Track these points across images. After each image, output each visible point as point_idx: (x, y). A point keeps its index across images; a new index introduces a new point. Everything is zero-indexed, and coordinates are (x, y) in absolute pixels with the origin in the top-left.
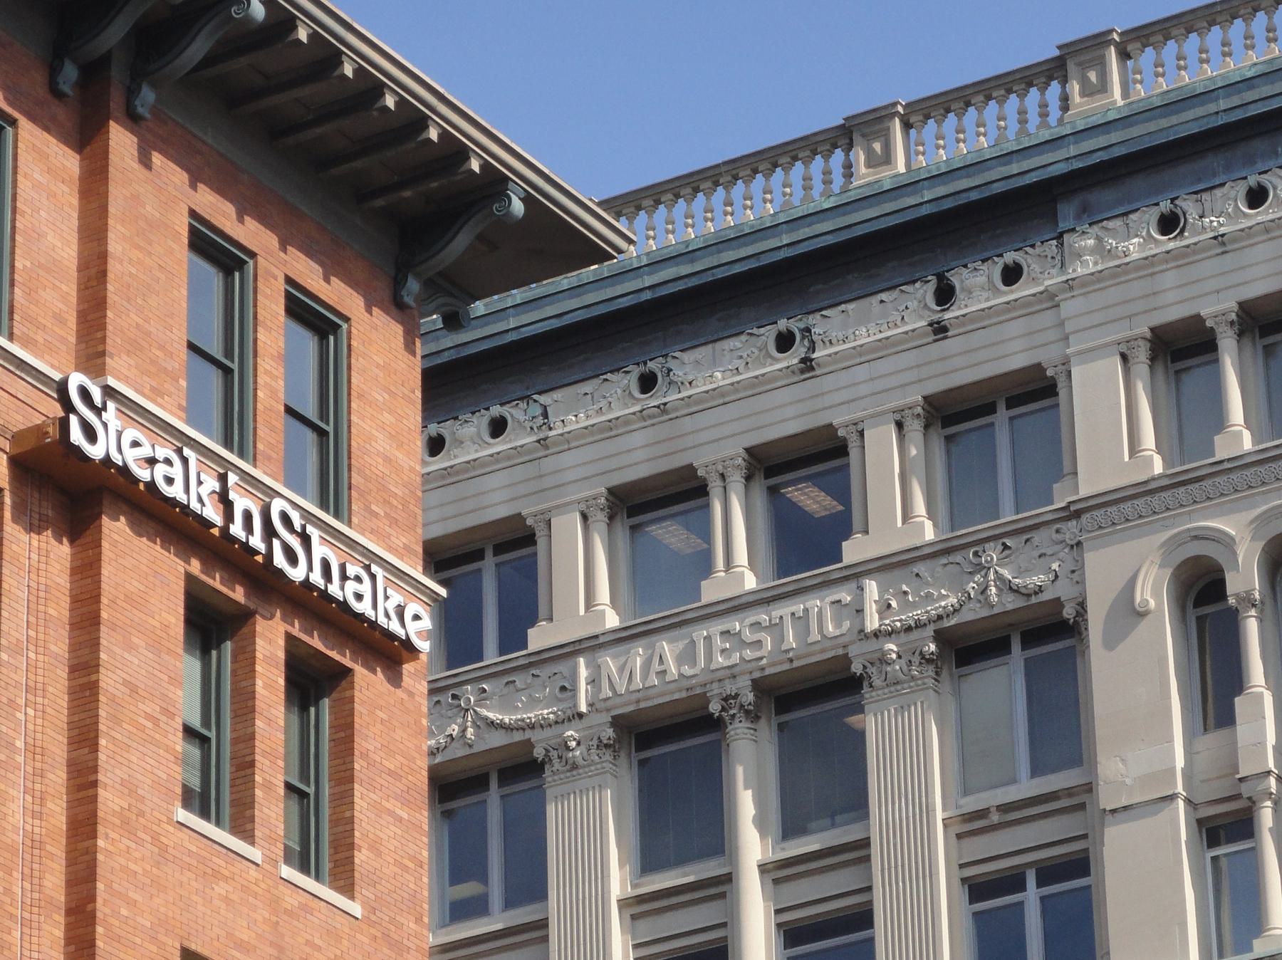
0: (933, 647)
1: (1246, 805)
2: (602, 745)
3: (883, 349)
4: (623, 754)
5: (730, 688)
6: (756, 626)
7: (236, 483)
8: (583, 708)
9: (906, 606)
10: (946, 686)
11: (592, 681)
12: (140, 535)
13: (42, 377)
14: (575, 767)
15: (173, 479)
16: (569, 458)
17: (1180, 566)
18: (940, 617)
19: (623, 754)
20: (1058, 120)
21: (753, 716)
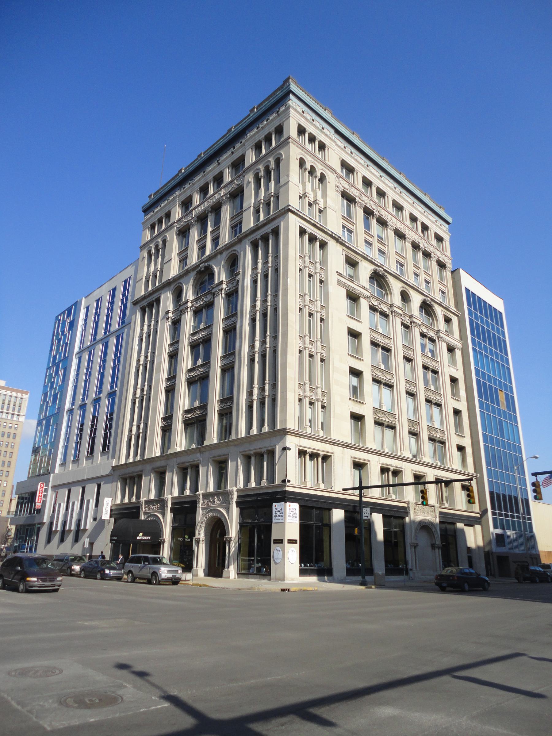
0: (229, 196)
1: (450, 222)
2: (196, 221)
3: (274, 119)
4: (199, 223)
5: (208, 209)
6: (211, 199)
7: (329, 241)
8: (193, 216)
9: (226, 191)
10: (231, 201)
11: (195, 213)
12: (188, 275)
13: (291, 541)
14: (193, 225)
15: (360, 334)
16: (196, 185)
17: (266, 166)
18: (229, 191)
19: (199, 223)
20: (56, 317)
21: (211, 212)
